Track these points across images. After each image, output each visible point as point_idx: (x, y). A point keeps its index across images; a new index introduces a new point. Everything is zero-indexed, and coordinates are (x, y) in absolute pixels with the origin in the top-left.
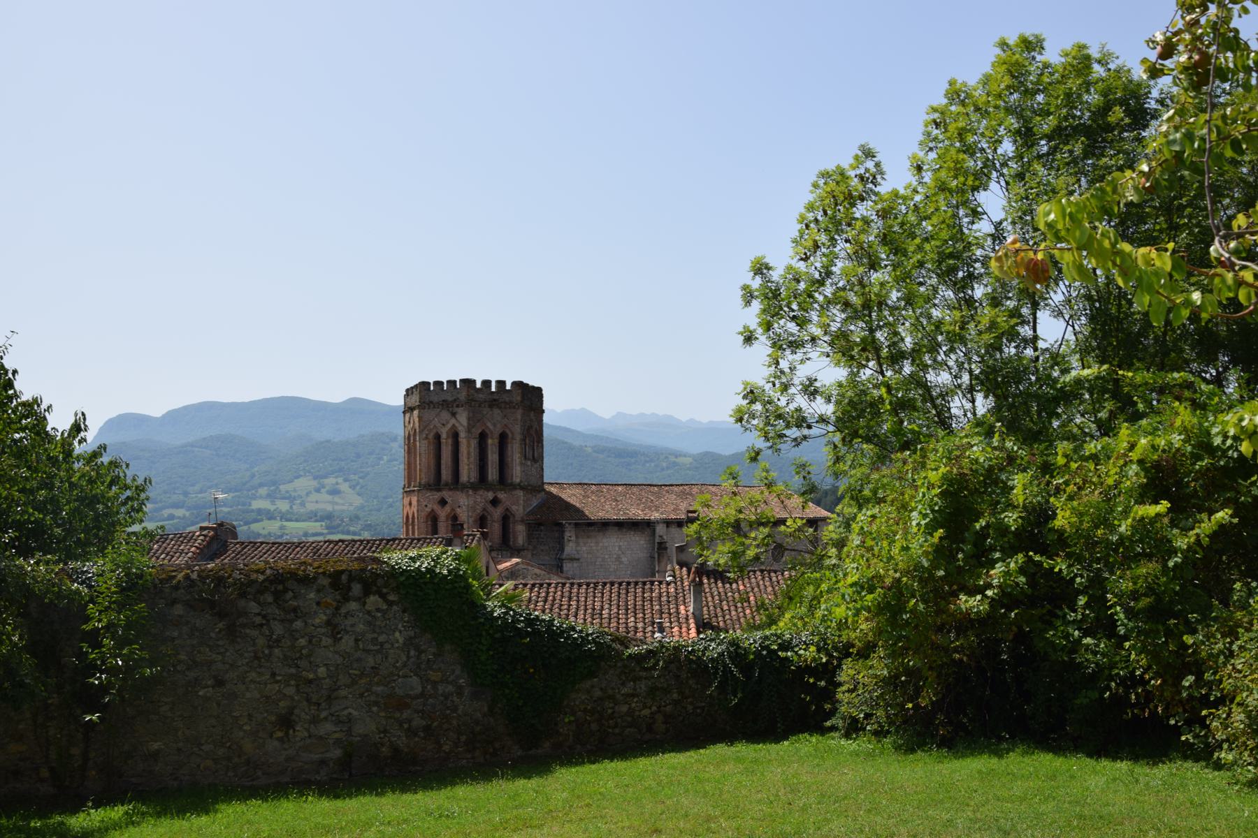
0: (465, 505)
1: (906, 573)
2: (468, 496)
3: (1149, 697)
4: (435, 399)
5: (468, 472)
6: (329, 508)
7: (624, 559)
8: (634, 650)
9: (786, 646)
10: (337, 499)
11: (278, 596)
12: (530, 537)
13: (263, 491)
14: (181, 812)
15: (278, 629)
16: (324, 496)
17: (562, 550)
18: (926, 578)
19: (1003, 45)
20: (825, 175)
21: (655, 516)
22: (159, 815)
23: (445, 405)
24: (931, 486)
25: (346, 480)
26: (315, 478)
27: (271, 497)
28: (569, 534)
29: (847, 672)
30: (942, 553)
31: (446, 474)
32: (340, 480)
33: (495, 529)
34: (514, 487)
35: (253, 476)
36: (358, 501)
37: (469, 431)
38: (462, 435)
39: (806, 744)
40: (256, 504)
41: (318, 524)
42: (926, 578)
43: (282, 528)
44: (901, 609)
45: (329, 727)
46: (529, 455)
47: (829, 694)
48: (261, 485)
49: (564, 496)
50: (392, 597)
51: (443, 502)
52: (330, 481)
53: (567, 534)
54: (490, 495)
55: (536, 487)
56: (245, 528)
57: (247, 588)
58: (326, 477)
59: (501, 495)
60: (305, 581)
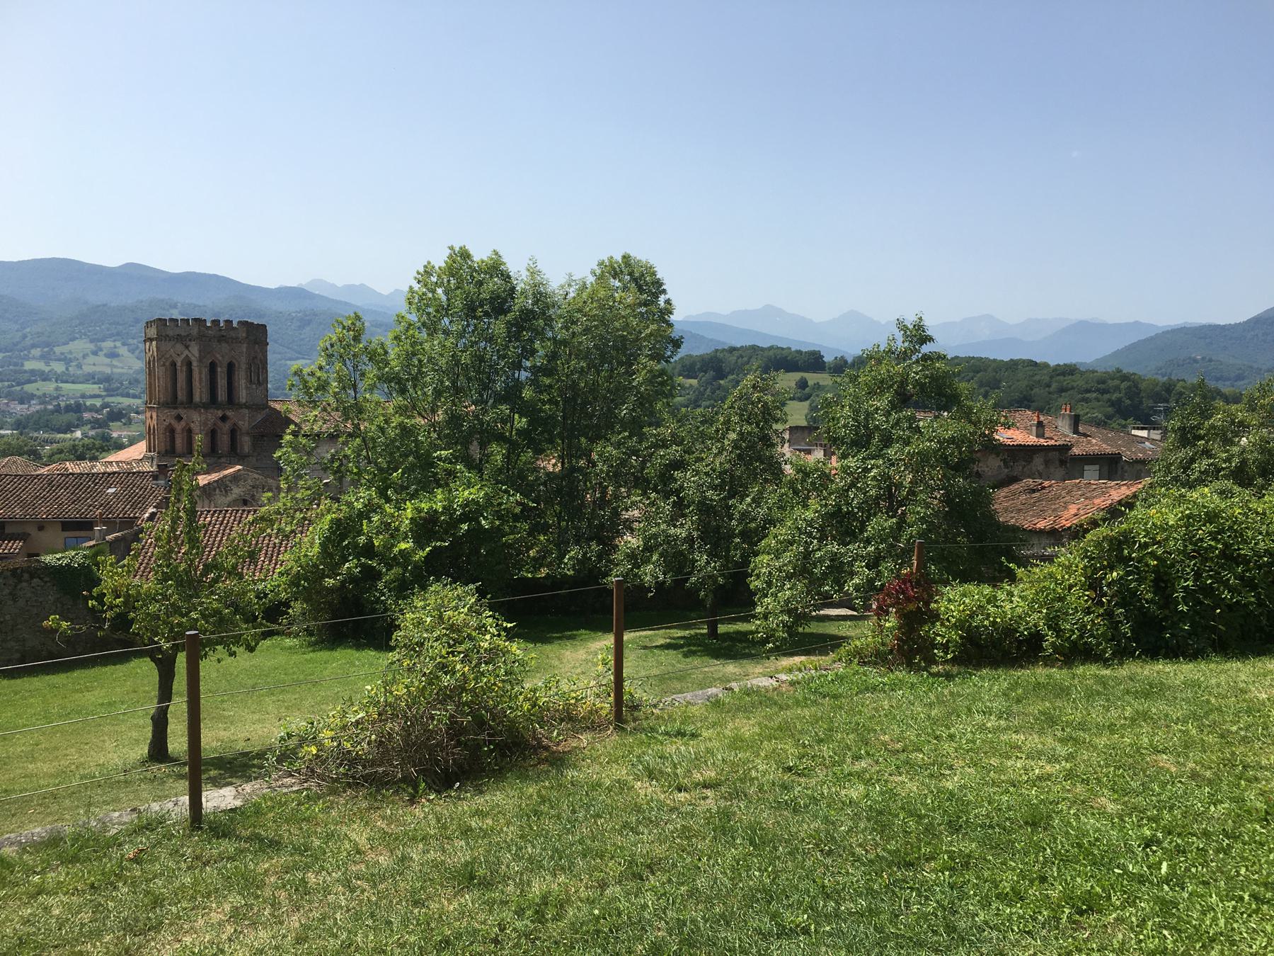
0: (197, 420)
2: (200, 414)
4: (171, 333)
5: (200, 394)
6: (108, 371)
10: (115, 362)
12: (254, 446)
16: (101, 359)
19: (451, 248)
25: (124, 344)
26: (91, 341)
27: (45, 358)
31: (181, 395)
32: (118, 344)
33: (224, 440)
34: (241, 406)
35: (25, 337)
37: (200, 360)
38: (195, 364)
40: (29, 365)
41: (96, 386)
43: (57, 389)
45: (13, 643)
48: (34, 346)
50: (46, 579)
51: (179, 418)
52: (108, 344)
54: (220, 413)
56: (18, 388)
59: (229, 413)
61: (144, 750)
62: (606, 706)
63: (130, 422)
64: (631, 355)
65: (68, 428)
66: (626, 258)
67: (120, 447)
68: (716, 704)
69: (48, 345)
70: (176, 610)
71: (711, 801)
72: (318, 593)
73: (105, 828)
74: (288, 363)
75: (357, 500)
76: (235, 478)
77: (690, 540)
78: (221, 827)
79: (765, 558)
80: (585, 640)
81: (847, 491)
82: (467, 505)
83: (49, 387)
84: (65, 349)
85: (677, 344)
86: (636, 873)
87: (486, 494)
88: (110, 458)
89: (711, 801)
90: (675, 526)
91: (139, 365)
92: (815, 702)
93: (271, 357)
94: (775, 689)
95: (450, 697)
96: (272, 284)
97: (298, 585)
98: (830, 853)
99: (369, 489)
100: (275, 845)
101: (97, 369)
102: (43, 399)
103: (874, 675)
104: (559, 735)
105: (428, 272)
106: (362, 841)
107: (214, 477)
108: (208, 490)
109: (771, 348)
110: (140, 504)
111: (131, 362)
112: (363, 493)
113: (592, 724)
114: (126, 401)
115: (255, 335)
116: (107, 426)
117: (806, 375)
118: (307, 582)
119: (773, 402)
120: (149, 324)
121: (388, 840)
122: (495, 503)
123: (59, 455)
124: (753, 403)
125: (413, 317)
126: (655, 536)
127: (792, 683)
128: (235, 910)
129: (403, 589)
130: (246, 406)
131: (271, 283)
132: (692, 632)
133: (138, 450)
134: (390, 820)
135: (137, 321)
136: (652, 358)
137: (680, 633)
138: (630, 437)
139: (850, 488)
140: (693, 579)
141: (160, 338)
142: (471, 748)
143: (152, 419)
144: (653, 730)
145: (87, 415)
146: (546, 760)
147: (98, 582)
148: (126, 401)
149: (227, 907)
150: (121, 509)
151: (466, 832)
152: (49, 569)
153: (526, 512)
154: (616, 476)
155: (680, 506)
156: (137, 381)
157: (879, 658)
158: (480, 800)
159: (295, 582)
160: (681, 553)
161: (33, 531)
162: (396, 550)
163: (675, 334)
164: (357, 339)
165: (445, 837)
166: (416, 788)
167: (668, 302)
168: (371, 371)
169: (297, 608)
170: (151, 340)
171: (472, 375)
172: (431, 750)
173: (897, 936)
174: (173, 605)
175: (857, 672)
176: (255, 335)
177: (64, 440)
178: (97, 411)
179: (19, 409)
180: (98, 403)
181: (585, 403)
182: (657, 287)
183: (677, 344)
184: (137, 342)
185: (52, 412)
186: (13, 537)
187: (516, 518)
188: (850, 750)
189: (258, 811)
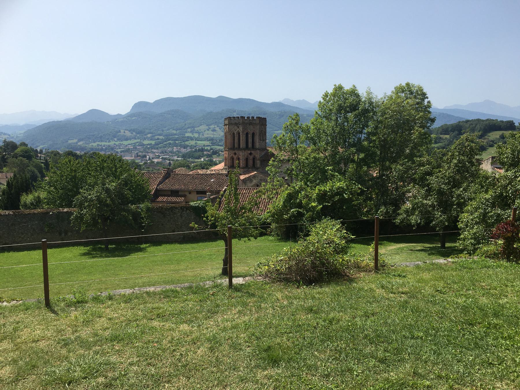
0: (242, 155)
4: (233, 122)
5: (243, 145)
6: (212, 136)
10: (215, 133)
11: (172, 211)
12: (261, 164)
13: (189, 130)
14: (157, 246)
16: (210, 132)
19: (335, 85)
22: (153, 246)
23: (236, 124)
25: (218, 126)
26: (207, 126)
27: (192, 132)
31: (236, 145)
32: (216, 126)
33: (251, 163)
34: (256, 149)
35: (186, 124)
37: (243, 132)
38: (241, 133)
40: (187, 135)
46: (262, 139)
48: (189, 128)
51: (235, 154)
52: (212, 126)
54: (249, 152)
59: (252, 152)
61: (220, 271)
62: (372, 264)
63: (219, 155)
64: (411, 126)
65: (199, 158)
66: (408, 84)
67: (216, 164)
68: (418, 267)
70: (231, 223)
71: (404, 297)
72: (281, 220)
73: (204, 286)
74: (275, 132)
75: (296, 186)
76: (254, 176)
77: (433, 206)
78: (238, 289)
79: (466, 215)
80: (387, 245)
81: (507, 186)
82: (339, 189)
83: (193, 143)
85: (433, 120)
86: (366, 315)
87: (346, 184)
88: (212, 169)
89: (404, 297)
90: (426, 200)
91: (222, 134)
92: (460, 270)
93: (268, 130)
94: (445, 264)
95: (312, 254)
96: (270, 102)
97: (274, 217)
98: (442, 318)
99: (301, 181)
100: (253, 295)
102: (191, 147)
103: (490, 262)
104: (353, 272)
105: (326, 95)
106: (280, 297)
107: (247, 176)
108: (244, 181)
109: (487, 120)
110: (221, 185)
111: (220, 133)
112: (299, 183)
113: (366, 270)
114: (218, 148)
115: (262, 122)
116: (212, 157)
117: (504, 132)
118: (277, 216)
119: (475, 146)
120: (225, 119)
121: (287, 298)
122: (350, 188)
123: (196, 167)
124: (465, 147)
125: (320, 113)
126: (417, 203)
127: (453, 262)
128: (239, 311)
129: (312, 220)
131: (269, 101)
132: (434, 245)
133: (221, 166)
134: (289, 292)
135: (222, 117)
136: (420, 127)
137: (428, 245)
138: (408, 162)
139: (508, 184)
140: (434, 223)
141: (230, 124)
142: (319, 272)
143: (225, 154)
144: (389, 273)
145: (205, 153)
146: (347, 280)
147: (206, 212)
148: (218, 148)
149: (237, 310)
150: (215, 187)
151: (313, 298)
152: (192, 206)
153: (362, 192)
154: (401, 178)
155: (429, 191)
156: (222, 140)
157: (494, 256)
158: (320, 290)
159: (273, 216)
160: (429, 211)
161: (187, 194)
162: (310, 205)
163: (432, 117)
164: (297, 123)
165: (306, 298)
166: (299, 284)
167: (429, 102)
168: (303, 136)
169: (273, 226)
170: (226, 125)
171: (341, 136)
172: (305, 272)
173: (455, 343)
174: (230, 221)
175: (483, 260)
176: (262, 122)
177: (198, 162)
178: (209, 151)
179: (183, 150)
180: (209, 148)
181: (390, 147)
182: (424, 96)
183: (433, 120)
184: (222, 125)
185: (194, 152)
186: (181, 196)
187: (359, 194)
188: (466, 286)
189: (249, 285)
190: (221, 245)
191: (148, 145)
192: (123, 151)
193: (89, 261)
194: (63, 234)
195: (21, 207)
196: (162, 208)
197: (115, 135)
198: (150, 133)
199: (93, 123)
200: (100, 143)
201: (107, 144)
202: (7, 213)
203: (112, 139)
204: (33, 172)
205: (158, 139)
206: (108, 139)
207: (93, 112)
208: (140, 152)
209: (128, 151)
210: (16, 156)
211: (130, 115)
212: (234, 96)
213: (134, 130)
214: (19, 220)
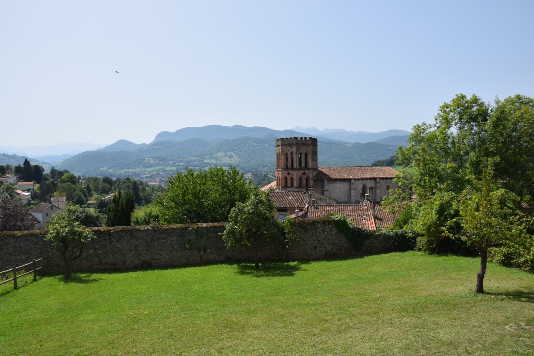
0: (296, 175)
1: (432, 222)
3: (475, 246)
4: (286, 143)
5: (296, 165)
6: (229, 162)
7: (342, 190)
8: (376, 234)
9: (406, 233)
10: (231, 159)
11: (314, 225)
12: (314, 184)
15: (314, 231)
16: (228, 158)
17: (324, 187)
18: (435, 223)
20: (415, 127)
21: (351, 177)
23: (289, 145)
24: (437, 205)
25: (234, 153)
28: (326, 183)
29: (419, 239)
30: (439, 219)
33: (304, 182)
34: (309, 169)
36: (238, 160)
37: (296, 153)
39: (409, 253)
40: (206, 161)
42: (435, 223)
44: (430, 229)
47: (415, 243)
48: (207, 155)
49: (323, 171)
51: (289, 174)
52: (229, 153)
53: (325, 183)
54: (303, 172)
55: (315, 169)
57: (309, 224)
58: (227, 152)
59: (306, 172)
60: (318, 222)
69: (211, 154)
84: (216, 155)
96: (282, 130)
101: (226, 161)
115: (313, 142)
120: (278, 140)
130: (312, 169)
141: (283, 145)
152: (334, 221)
170: (279, 146)
190: (477, 261)
191: (170, 171)
192: (148, 177)
193: (241, 277)
194: (202, 252)
195: (132, 224)
196: (304, 222)
197: (140, 162)
198: (172, 160)
199: (121, 152)
200: (127, 170)
201: (133, 170)
202: (146, 229)
203: (138, 166)
204: (79, 196)
205: (179, 165)
206: (134, 166)
207: (122, 142)
208: (163, 177)
209: (152, 177)
210: (63, 182)
211: (153, 144)
212: (249, 124)
213: (157, 158)
214: (158, 236)
